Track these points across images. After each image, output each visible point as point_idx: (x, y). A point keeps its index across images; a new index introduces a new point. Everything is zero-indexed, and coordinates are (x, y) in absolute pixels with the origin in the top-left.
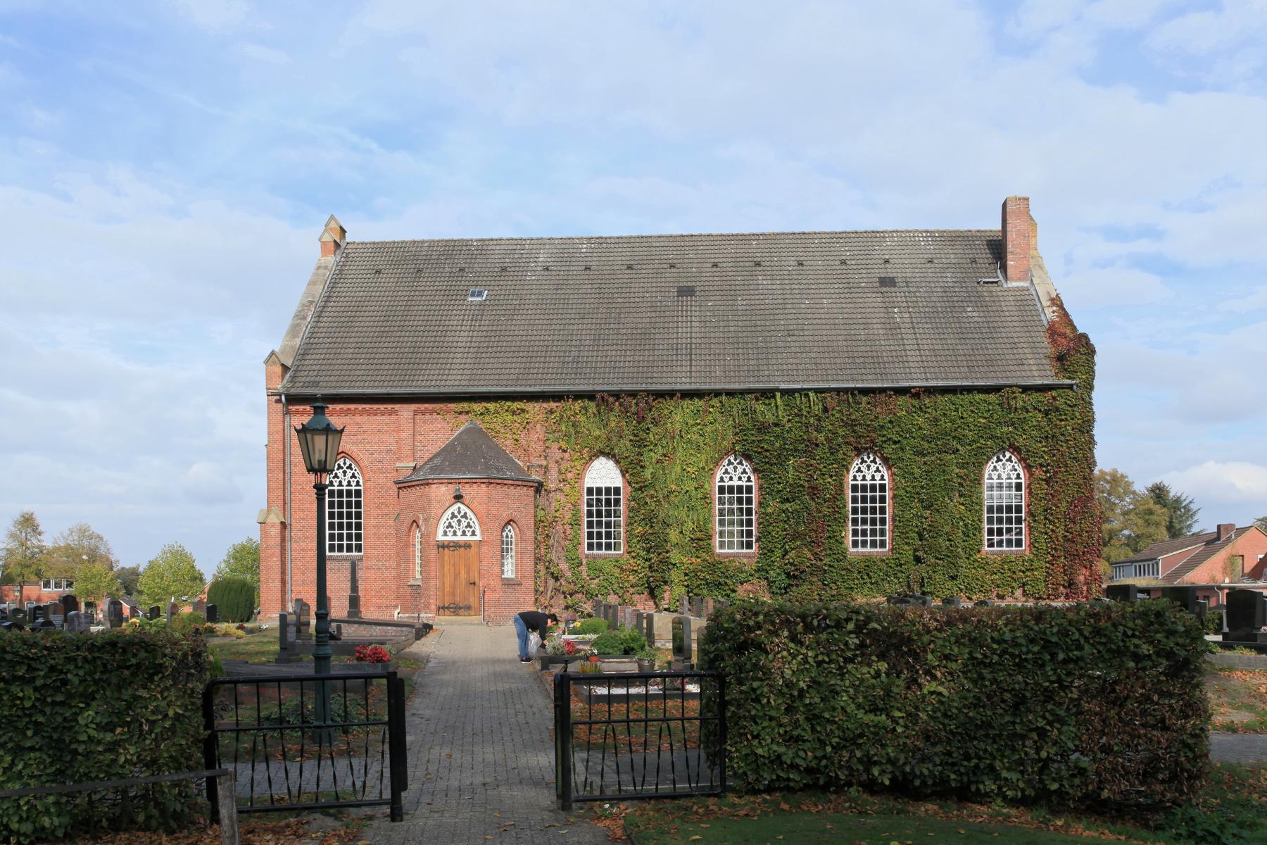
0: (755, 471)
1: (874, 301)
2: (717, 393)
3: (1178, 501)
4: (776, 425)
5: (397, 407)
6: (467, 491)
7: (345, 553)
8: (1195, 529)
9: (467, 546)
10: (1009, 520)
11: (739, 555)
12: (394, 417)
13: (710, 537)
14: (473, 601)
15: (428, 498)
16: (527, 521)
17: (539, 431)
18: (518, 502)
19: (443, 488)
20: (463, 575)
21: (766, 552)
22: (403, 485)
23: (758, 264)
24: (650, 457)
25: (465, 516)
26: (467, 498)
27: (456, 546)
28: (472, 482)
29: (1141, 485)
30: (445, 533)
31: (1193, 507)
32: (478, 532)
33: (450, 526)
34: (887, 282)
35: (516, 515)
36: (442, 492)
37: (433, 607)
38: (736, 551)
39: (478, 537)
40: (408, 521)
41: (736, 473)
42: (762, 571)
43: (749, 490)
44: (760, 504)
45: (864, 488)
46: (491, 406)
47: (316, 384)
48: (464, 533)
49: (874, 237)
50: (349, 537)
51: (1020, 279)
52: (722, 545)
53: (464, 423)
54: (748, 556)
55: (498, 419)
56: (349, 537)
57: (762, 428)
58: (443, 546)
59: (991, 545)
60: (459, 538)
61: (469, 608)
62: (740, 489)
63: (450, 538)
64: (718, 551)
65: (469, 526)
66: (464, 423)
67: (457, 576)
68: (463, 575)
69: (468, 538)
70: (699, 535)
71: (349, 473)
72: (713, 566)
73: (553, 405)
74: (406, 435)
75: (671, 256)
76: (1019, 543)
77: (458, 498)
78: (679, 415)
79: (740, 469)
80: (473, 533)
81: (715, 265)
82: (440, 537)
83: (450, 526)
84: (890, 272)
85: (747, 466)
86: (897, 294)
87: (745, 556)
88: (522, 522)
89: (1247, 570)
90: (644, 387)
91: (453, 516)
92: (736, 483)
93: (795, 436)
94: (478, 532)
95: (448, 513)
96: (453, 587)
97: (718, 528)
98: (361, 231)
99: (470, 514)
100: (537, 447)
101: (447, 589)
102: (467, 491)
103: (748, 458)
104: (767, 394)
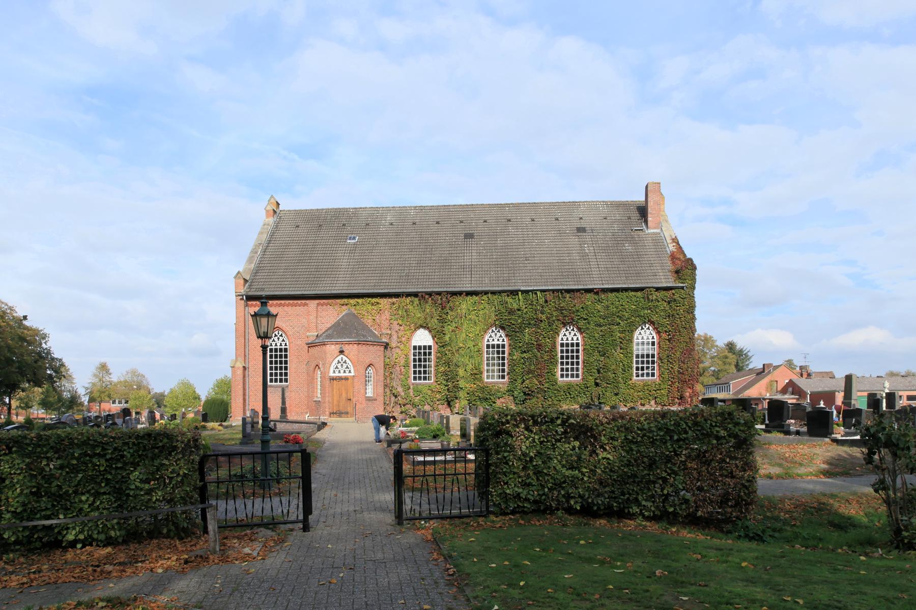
0: (507, 335)
1: (574, 240)
2: (486, 293)
3: (741, 351)
4: (519, 310)
5: (307, 302)
6: (346, 348)
7: (278, 383)
8: (751, 367)
9: (346, 379)
10: (648, 362)
11: (497, 383)
12: (306, 307)
13: (481, 373)
14: (349, 409)
15: (325, 353)
16: (380, 364)
17: (387, 315)
18: (374, 354)
19: (333, 347)
20: (344, 395)
21: (513, 381)
22: (311, 345)
23: (509, 220)
24: (448, 329)
25: (345, 362)
26: (346, 352)
27: (341, 379)
28: (349, 343)
29: (721, 342)
30: (334, 372)
31: (750, 354)
32: (352, 371)
33: (337, 368)
34: (581, 230)
35: (374, 361)
36: (332, 349)
37: (327, 413)
38: (496, 380)
39: (352, 374)
40: (313, 365)
41: (497, 337)
42: (510, 391)
43: (503, 346)
44: (510, 354)
45: (567, 345)
46: (360, 301)
47: (263, 290)
48: (345, 372)
49: (574, 205)
50: (281, 374)
51: (655, 228)
52: (488, 377)
53: (345, 311)
54: (503, 383)
55: (364, 308)
56: (281, 374)
57: (511, 312)
58: (333, 379)
59: (638, 376)
60: (342, 374)
61: (347, 413)
62: (498, 346)
63: (337, 374)
64: (486, 380)
65: (347, 367)
66: (345, 311)
67: (340, 395)
68: (344, 395)
69: (347, 374)
70: (475, 371)
71: (281, 339)
72: (483, 389)
73: (394, 300)
74: (312, 318)
75: (461, 216)
76: (653, 375)
77: (342, 352)
78: (464, 305)
79: (498, 335)
80: (350, 372)
81: (485, 221)
82: (332, 374)
83: (337, 368)
84: (583, 224)
85: (502, 333)
86: (587, 237)
87: (501, 383)
88: (377, 365)
89: (779, 389)
90: (445, 289)
91: (339, 362)
92: (496, 342)
93: (529, 317)
94: (352, 371)
95: (336, 361)
96: (339, 402)
97: (486, 368)
98: (288, 204)
99: (348, 361)
100: (385, 324)
101: (335, 402)
102: (346, 348)
103: (503, 328)
104: (514, 293)
